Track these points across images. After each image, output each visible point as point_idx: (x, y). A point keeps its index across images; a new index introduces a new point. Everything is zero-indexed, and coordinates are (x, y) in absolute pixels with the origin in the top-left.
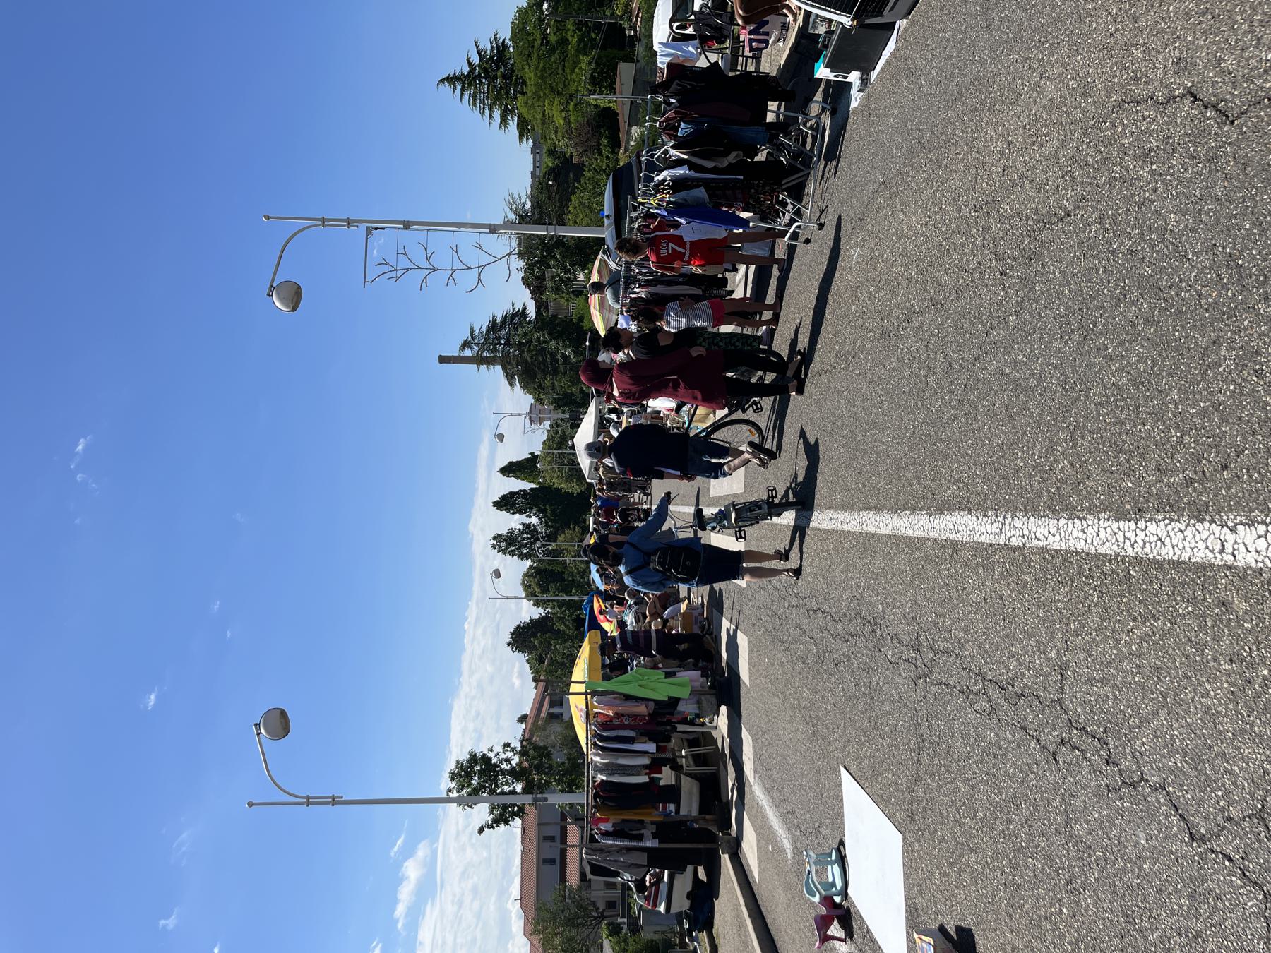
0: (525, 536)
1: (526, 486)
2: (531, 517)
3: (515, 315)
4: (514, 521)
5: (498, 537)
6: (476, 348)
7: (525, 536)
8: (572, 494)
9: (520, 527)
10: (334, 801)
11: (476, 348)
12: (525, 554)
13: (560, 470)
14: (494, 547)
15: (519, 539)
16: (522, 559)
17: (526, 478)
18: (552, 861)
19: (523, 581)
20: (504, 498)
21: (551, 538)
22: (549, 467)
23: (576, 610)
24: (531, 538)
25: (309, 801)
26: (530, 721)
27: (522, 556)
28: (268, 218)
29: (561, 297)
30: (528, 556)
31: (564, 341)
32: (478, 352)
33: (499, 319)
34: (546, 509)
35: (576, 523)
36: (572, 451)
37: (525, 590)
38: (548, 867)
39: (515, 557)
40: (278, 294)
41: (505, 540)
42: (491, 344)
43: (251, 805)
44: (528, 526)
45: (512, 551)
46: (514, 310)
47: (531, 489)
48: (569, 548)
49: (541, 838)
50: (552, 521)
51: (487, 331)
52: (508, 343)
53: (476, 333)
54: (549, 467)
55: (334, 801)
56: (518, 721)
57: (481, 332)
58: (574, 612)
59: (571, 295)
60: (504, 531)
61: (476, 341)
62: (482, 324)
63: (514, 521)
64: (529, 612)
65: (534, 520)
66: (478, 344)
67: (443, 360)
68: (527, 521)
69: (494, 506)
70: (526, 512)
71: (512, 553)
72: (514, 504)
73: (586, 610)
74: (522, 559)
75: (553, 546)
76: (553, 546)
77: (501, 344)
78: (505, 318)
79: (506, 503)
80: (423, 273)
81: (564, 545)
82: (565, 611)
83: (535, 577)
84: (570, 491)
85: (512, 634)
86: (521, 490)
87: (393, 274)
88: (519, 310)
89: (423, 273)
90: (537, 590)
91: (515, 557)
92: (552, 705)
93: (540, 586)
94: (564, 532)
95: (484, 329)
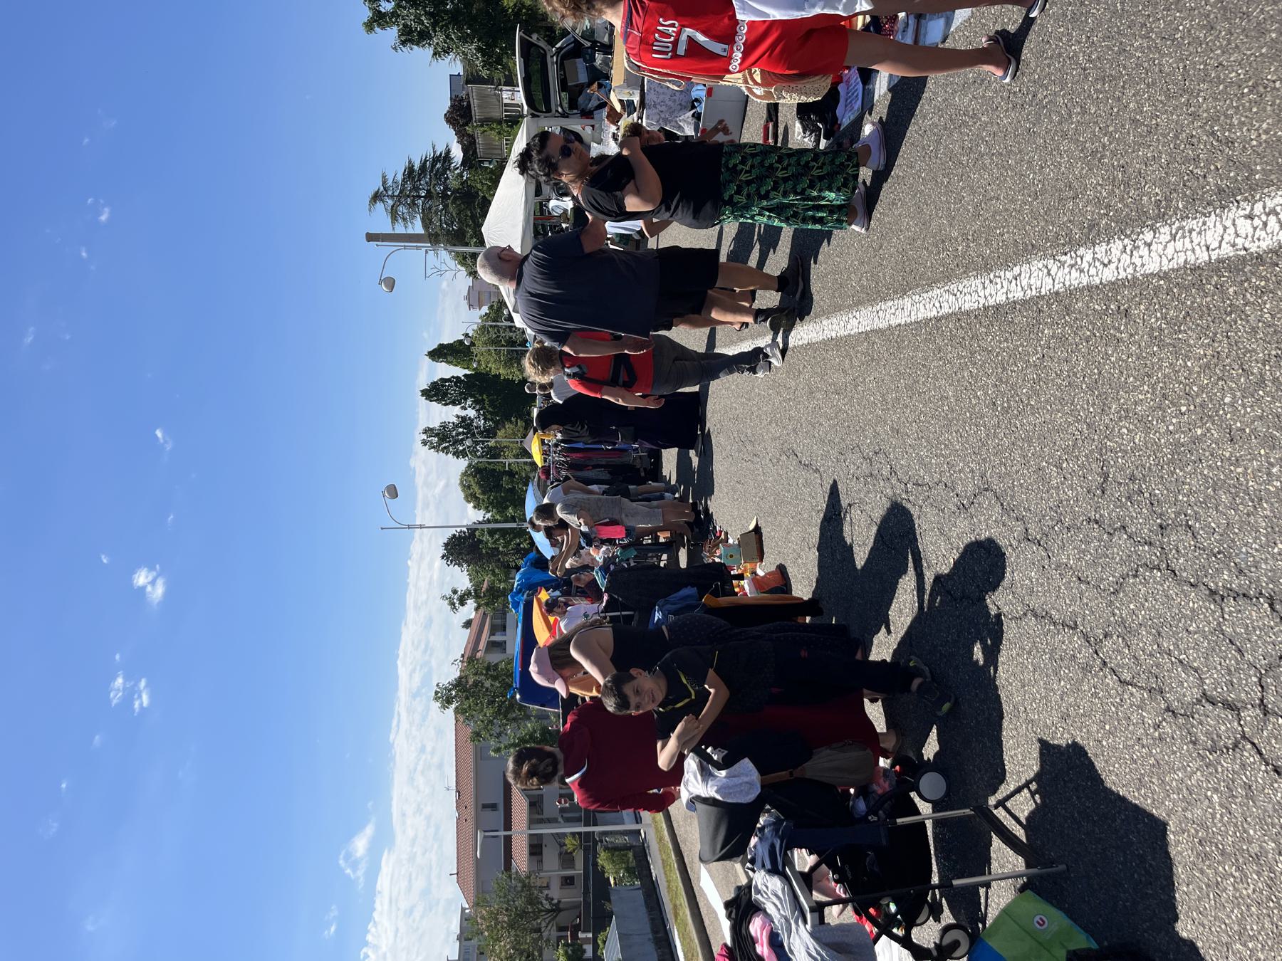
0: (461, 430)
1: (460, 372)
2: (466, 409)
3: (436, 159)
4: (447, 414)
5: (428, 431)
6: (390, 202)
7: (461, 430)
9: (455, 420)
11: (390, 202)
13: (498, 353)
14: (424, 443)
15: (454, 434)
16: (458, 457)
17: (459, 363)
18: (493, 807)
19: (462, 482)
21: (489, 433)
22: (484, 349)
23: (515, 538)
24: (467, 433)
26: (475, 625)
27: (457, 454)
29: (492, 129)
30: (463, 454)
31: (460, 29)
32: (393, 207)
33: (417, 166)
34: (483, 400)
35: (520, 416)
36: (509, 324)
37: (463, 490)
38: (489, 814)
39: (450, 455)
40: (385, 284)
41: (437, 435)
42: (408, 196)
43: (382, 529)
44: (464, 419)
45: (445, 448)
46: (434, 152)
47: (465, 376)
48: (511, 445)
49: (480, 807)
50: (491, 413)
51: (403, 180)
52: (429, 195)
53: (390, 182)
54: (484, 349)
56: (463, 627)
57: (394, 182)
58: (511, 540)
59: (504, 126)
60: (436, 424)
61: (390, 193)
62: (396, 172)
63: (447, 414)
64: (472, 515)
65: (471, 413)
66: (392, 197)
67: (371, 237)
68: (463, 413)
69: (422, 395)
70: (460, 404)
71: (446, 450)
72: (445, 394)
73: (516, 605)
74: (458, 457)
75: (492, 443)
76: (492, 443)
77: (420, 197)
78: (423, 167)
79: (436, 392)
81: (505, 442)
82: (498, 539)
83: (475, 476)
84: (510, 378)
85: (446, 545)
86: (453, 377)
88: (441, 154)
90: (477, 491)
91: (450, 455)
92: (493, 631)
93: (481, 486)
94: (504, 427)
95: (400, 178)
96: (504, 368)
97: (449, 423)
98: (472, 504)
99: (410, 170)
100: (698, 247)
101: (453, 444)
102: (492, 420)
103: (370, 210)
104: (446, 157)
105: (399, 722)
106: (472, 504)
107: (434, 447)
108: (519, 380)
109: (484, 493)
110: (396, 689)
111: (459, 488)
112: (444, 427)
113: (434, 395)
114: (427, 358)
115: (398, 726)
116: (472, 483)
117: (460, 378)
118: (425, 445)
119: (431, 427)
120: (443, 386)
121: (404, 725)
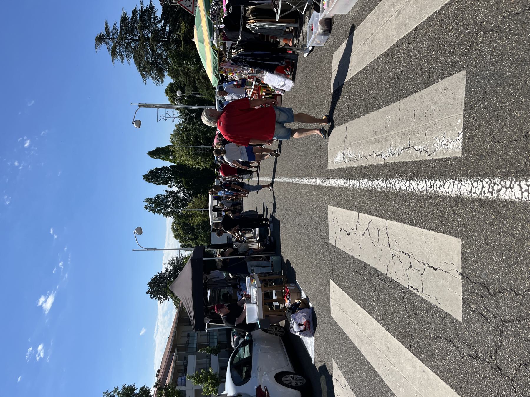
1: (168, 164)
2: (171, 187)
4: (161, 190)
5: (148, 200)
8: (199, 169)
9: (165, 193)
10: (154, 249)
12: (169, 212)
14: (146, 207)
16: (166, 216)
19: (173, 227)
20: (151, 172)
25: (148, 249)
28: (132, 104)
33: (130, 15)
39: (162, 215)
40: (136, 124)
43: (133, 250)
44: (171, 193)
45: (159, 210)
46: (142, 7)
47: (171, 166)
55: (154, 249)
60: (153, 196)
62: (115, 22)
63: (161, 190)
65: (175, 189)
68: (170, 189)
69: (144, 179)
70: (168, 183)
71: (159, 212)
72: (159, 178)
80: (173, 118)
81: (193, 211)
84: (197, 167)
86: (164, 167)
87: (165, 119)
89: (173, 118)
90: (182, 233)
91: (162, 215)
95: (118, 26)
96: (192, 160)
97: (162, 195)
98: (178, 240)
99: (124, 19)
100: (344, 50)
101: (164, 208)
102: (188, 193)
103: (96, 48)
104: (151, 10)
105: (158, 328)
106: (178, 240)
107: (152, 210)
108: (203, 169)
109: (185, 234)
110: (157, 313)
111: (171, 231)
112: (159, 198)
113: (152, 178)
114: (148, 155)
115: (157, 330)
116: (179, 228)
117: (168, 167)
118: (147, 209)
119: (150, 197)
120: (157, 173)
121: (160, 330)
